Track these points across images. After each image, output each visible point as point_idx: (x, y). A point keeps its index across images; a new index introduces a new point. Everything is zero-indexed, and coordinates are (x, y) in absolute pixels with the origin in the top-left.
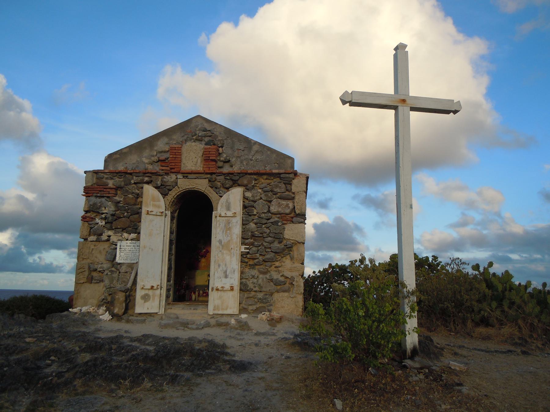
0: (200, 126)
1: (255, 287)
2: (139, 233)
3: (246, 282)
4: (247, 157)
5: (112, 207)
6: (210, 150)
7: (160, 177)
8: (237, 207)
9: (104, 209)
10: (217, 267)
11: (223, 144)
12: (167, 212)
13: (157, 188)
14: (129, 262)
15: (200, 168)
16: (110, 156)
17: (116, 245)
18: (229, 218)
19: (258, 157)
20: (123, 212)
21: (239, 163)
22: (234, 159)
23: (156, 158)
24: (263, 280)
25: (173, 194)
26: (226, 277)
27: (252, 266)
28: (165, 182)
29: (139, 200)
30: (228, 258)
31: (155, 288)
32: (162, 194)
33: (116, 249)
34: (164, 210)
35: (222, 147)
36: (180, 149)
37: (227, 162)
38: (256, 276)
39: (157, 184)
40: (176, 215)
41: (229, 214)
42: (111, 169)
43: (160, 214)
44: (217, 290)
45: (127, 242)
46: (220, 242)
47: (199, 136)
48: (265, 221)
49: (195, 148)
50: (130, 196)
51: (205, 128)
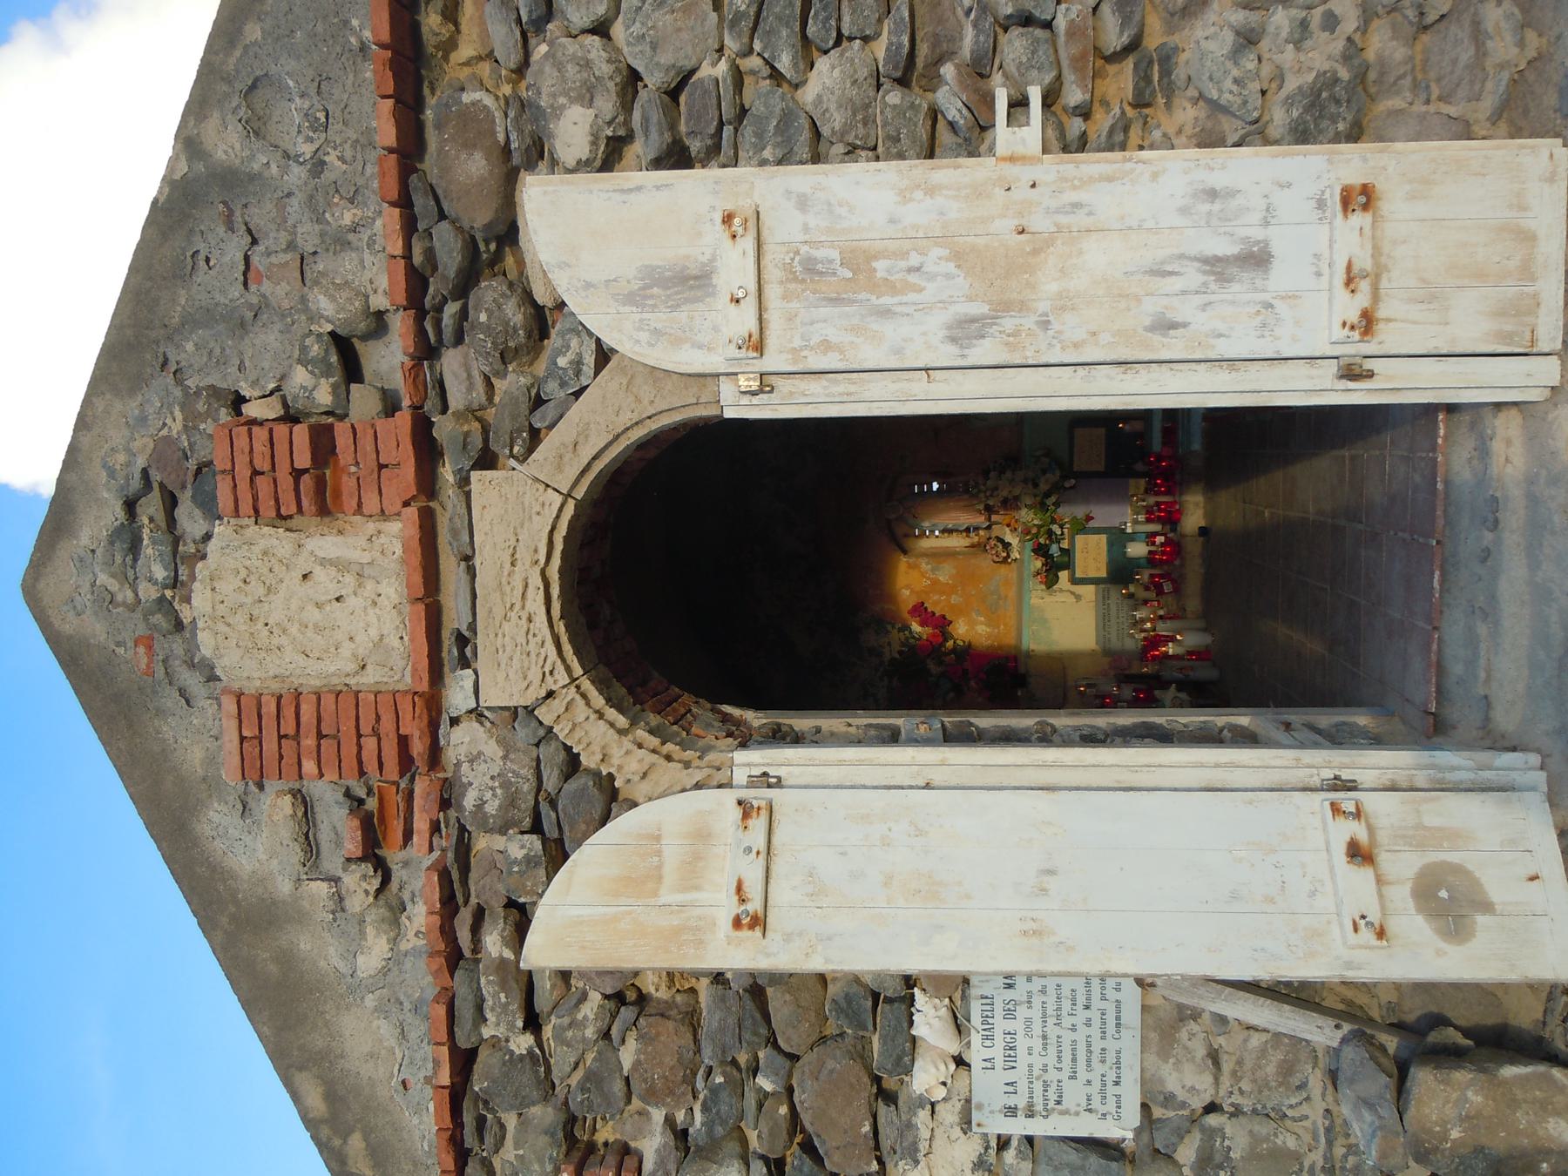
0: (103, 578)
1: (1331, 22)
2: (909, 981)
3: (1289, 102)
6: (243, 473)
7: (482, 843)
11: (214, 391)
12: (740, 776)
13: (557, 855)
14: (1130, 1043)
15: (396, 536)
17: (1003, 1143)
18: (772, 274)
19: (290, 114)
20: (751, 1101)
22: (323, 303)
25: (598, 733)
26: (1257, 259)
28: (511, 801)
29: (649, 985)
30: (1101, 258)
32: (604, 820)
33: (1030, 1140)
34: (729, 797)
35: (238, 401)
36: (247, 706)
37: (347, 359)
39: (529, 861)
40: (755, 719)
41: (735, 266)
44: (1367, 323)
45: (975, 1056)
46: (965, 330)
49: (228, 586)
50: (628, 1055)
51: (116, 535)
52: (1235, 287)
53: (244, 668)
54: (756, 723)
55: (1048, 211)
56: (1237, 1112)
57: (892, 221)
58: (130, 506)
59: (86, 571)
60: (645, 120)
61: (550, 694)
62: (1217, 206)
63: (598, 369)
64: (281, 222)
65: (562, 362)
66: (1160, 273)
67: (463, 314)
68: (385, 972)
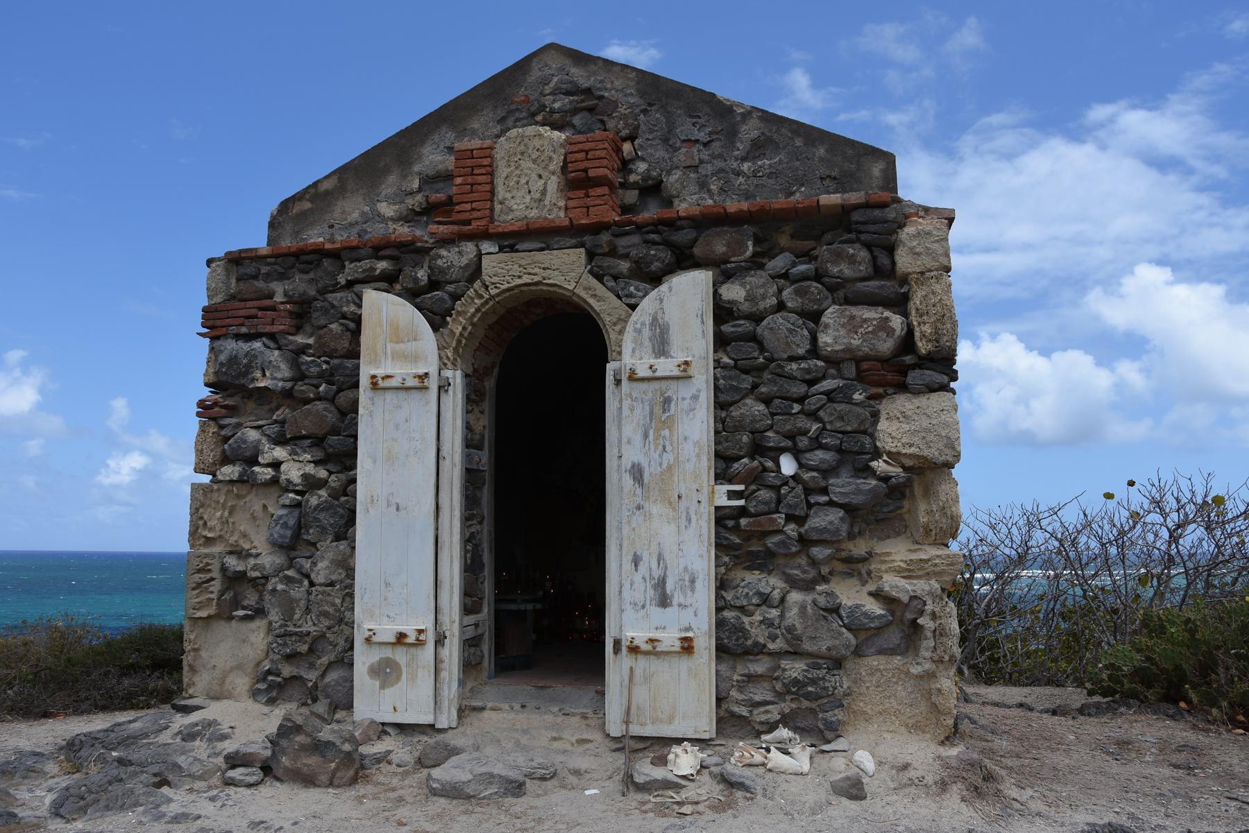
0: (556, 79)
1: (773, 638)
4: (720, 164)
5: (283, 366)
6: (588, 146)
8: (693, 338)
9: (258, 374)
10: (628, 566)
12: (448, 373)
15: (559, 216)
16: (285, 206)
18: (664, 384)
21: (693, 188)
23: (419, 197)
24: (803, 608)
25: (469, 307)
27: (763, 561)
28: (442, 271)
30: (667, 533)
31: (409, 640)
34: (433, 369)
35: (632, 138)
36: (488, 153)
38: (776, 595)
40: (490, 384)
41: (666, 367)
42: (287, 243)
43: (416, 383)
47: (552, 111)
48: (801, 389)
52: (652, 592)
53: (503, 147)
54: (487, 384)
55: (688, 508)
56: (309, 593)
57: (686, 438)
58: (588, 91)
59: (555, 71)
60: (740, 325)
61: (487, 287)
62: (687, 583)
63: (628, 305)
64: (713, 156)
65: (632, 289)
66: (660, 558)
67: (655, 243)
68: (379, 215)
